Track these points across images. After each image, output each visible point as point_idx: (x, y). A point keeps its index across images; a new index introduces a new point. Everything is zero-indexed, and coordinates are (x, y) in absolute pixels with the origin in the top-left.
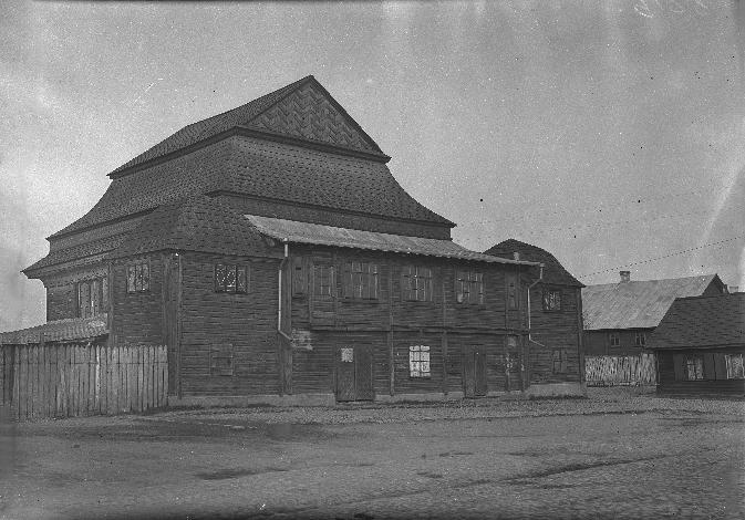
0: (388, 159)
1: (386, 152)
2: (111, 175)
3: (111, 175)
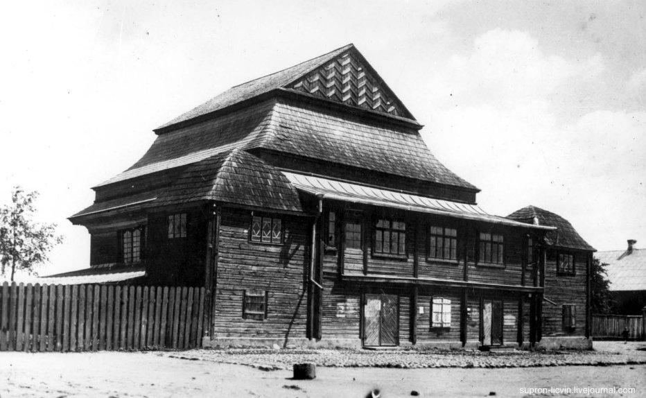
0: (420, 127)
2: (158, 132)
3: (158, 132)
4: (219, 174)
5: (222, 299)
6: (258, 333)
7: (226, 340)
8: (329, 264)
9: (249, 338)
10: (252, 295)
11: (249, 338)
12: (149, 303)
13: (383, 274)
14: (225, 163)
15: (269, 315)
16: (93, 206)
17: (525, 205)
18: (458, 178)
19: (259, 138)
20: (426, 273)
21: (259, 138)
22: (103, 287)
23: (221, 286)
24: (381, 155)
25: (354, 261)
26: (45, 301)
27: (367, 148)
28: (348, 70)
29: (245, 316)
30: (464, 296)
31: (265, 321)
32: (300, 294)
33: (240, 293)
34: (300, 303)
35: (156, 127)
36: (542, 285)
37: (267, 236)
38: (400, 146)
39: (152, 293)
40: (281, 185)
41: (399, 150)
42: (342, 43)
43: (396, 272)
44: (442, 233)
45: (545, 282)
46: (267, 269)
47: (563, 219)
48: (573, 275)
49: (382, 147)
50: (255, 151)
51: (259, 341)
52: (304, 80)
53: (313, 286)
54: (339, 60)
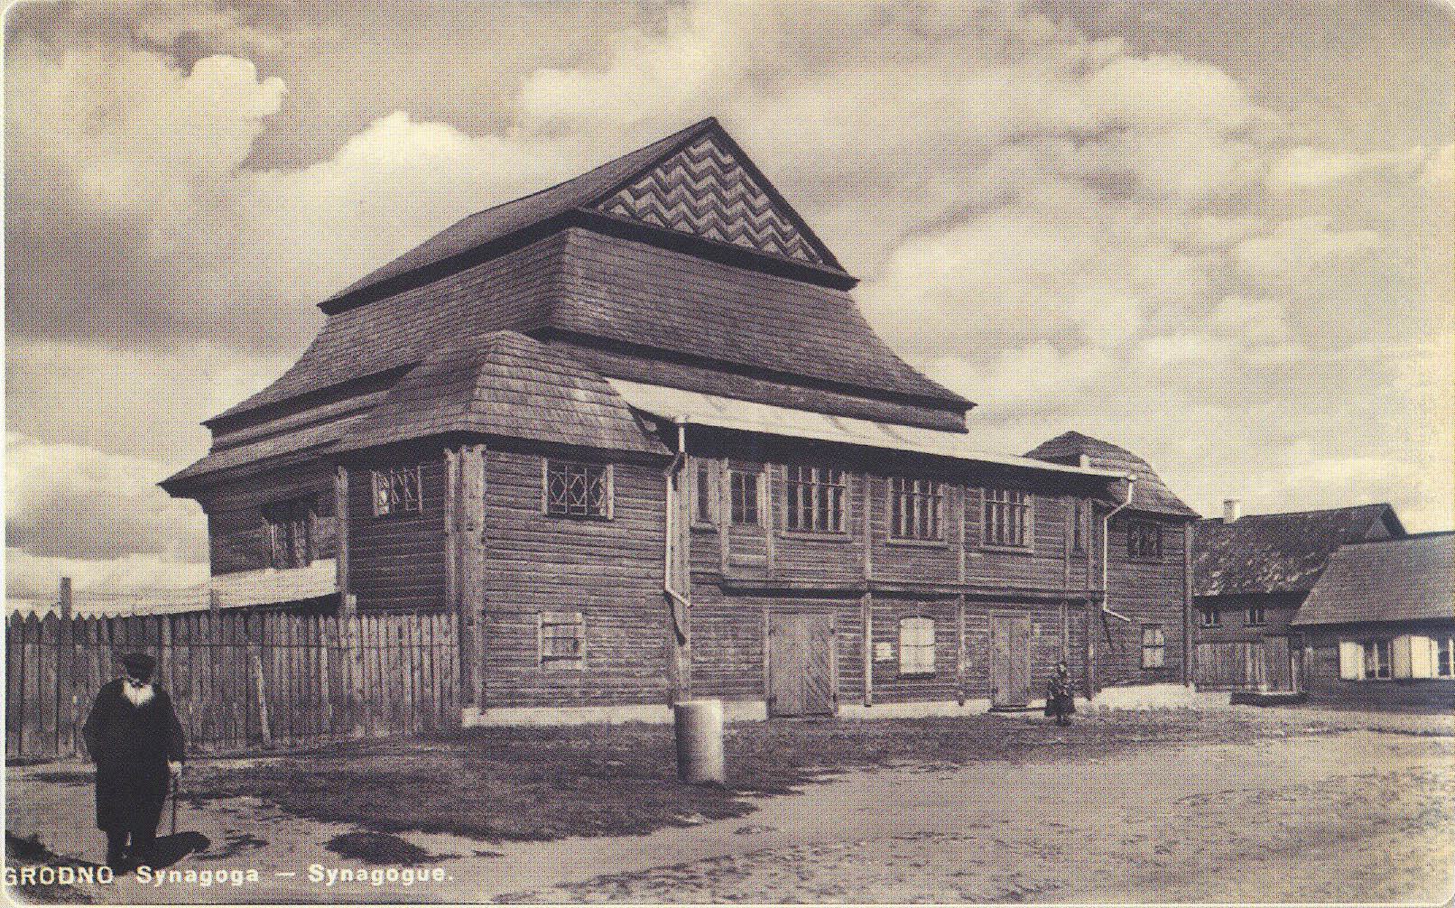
1: (852, 273)
12: (319, 647)
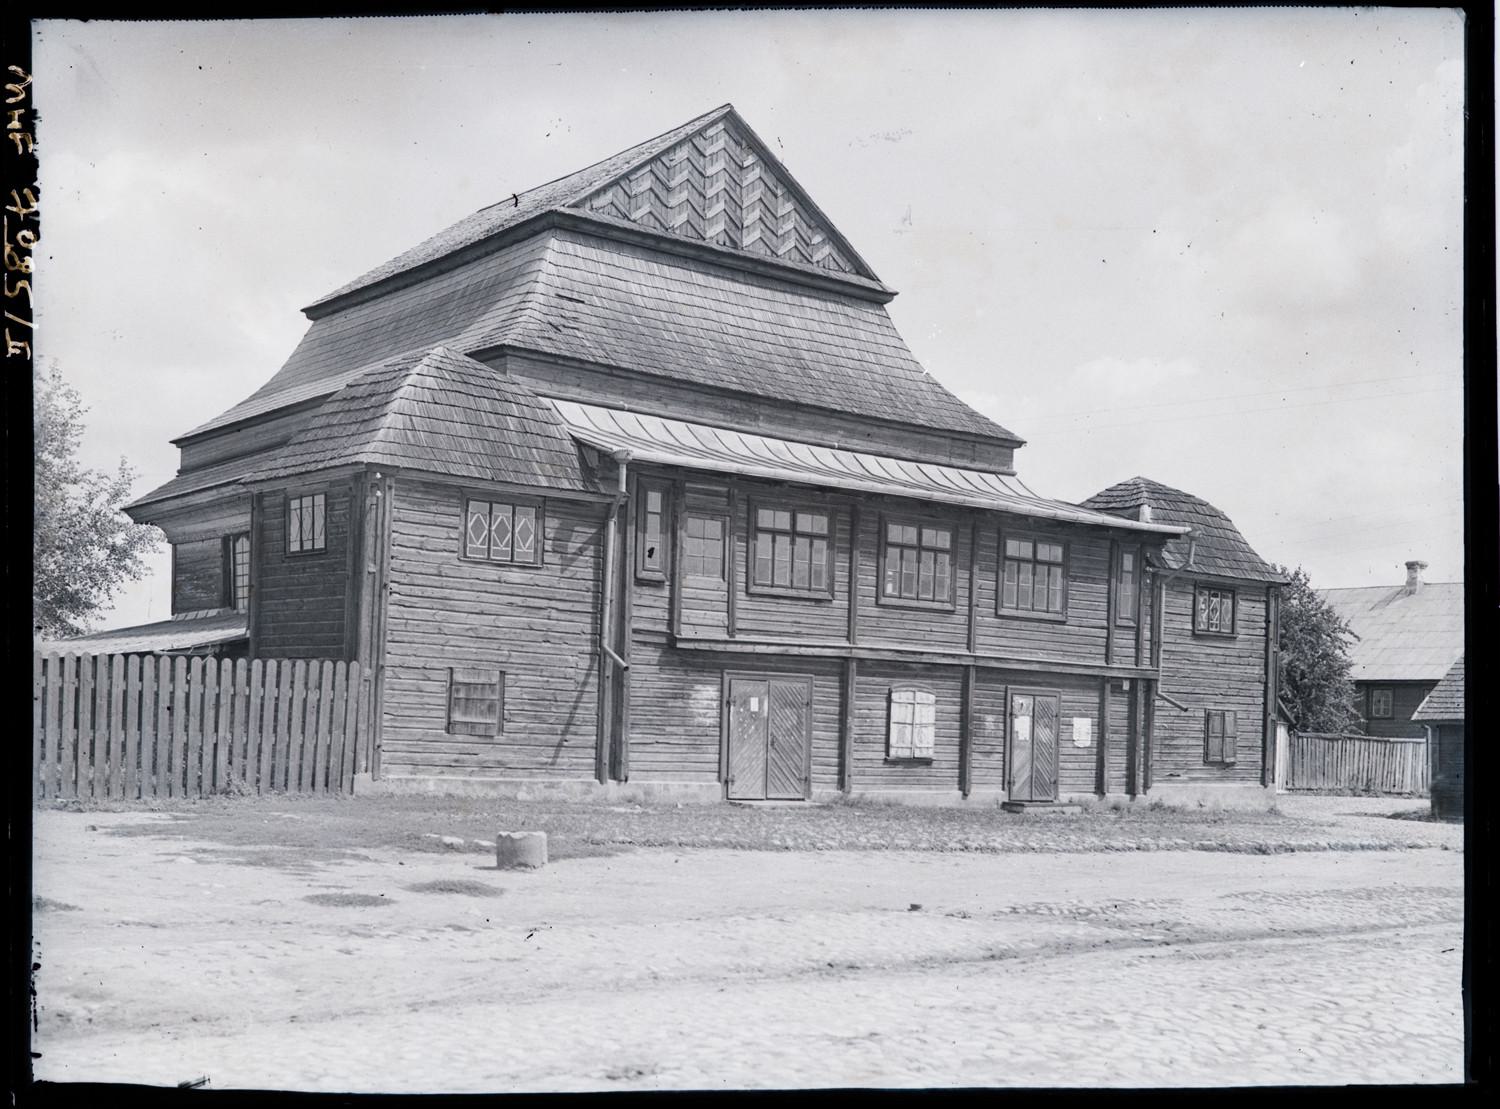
4: (394, 406)
5: (398, 690)
6: (484, 767)
7: (407, 780)
8: (647, 610)
9: (462, 778)
10: (467, 681)
11: (462, 778)
13: (774, 628)
14: (409, 380)
15: (507, 726)
16: (175, 481)
17: (1125, 476)
18: (972, 415)
19: (506, 326)
20: (877, 630)
21: (506, 326)
22: (131, 658)
23: (397, 660)
24: (792, 362)
25: (704, 604)
26: (117, 692)
27: (760, 346)
28: (720, 165)
29: (450, 727)
30: (970, 682)
31: (499, 738)
32: (581, 679)
33: (444, 676)
34: (578, 700)
35: (310, 302)
36: (1154, 660)
37: (502, 547)
38: (837, 341)
39: (241, 674)
40: (536, 430)
41: (835, 350)
42: (709, 103)
43: (804, 631)
44: (1030, 555)
45: (1162, 655)
46: (502, 621)
47: (1213, 509)
48: (1232, 638)
49: (795, 343)
50: (492, 354)
51: (482, 783)
52: (614, 189)
53: (608, 660)
54: (698, 141)
